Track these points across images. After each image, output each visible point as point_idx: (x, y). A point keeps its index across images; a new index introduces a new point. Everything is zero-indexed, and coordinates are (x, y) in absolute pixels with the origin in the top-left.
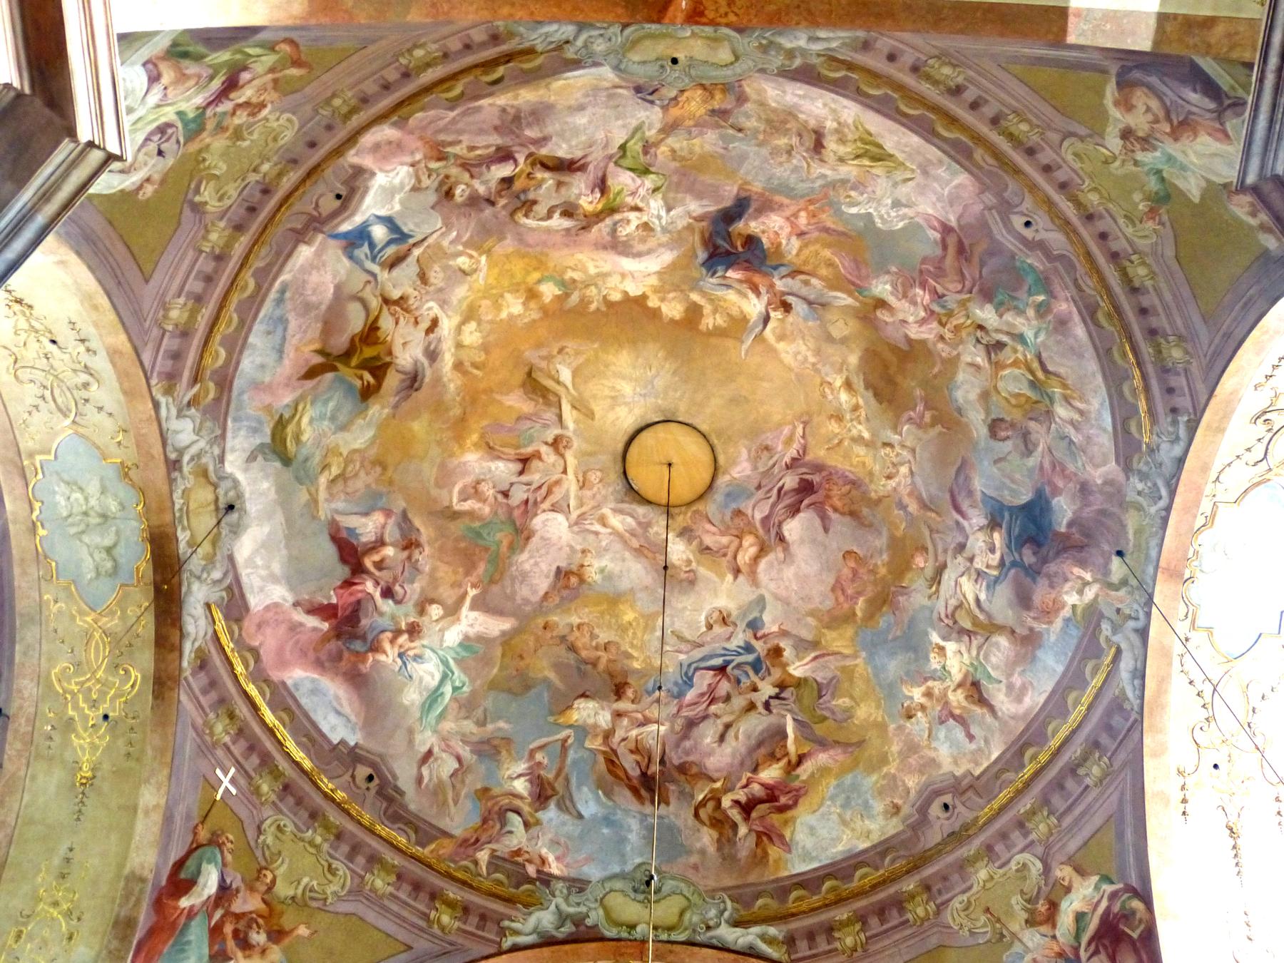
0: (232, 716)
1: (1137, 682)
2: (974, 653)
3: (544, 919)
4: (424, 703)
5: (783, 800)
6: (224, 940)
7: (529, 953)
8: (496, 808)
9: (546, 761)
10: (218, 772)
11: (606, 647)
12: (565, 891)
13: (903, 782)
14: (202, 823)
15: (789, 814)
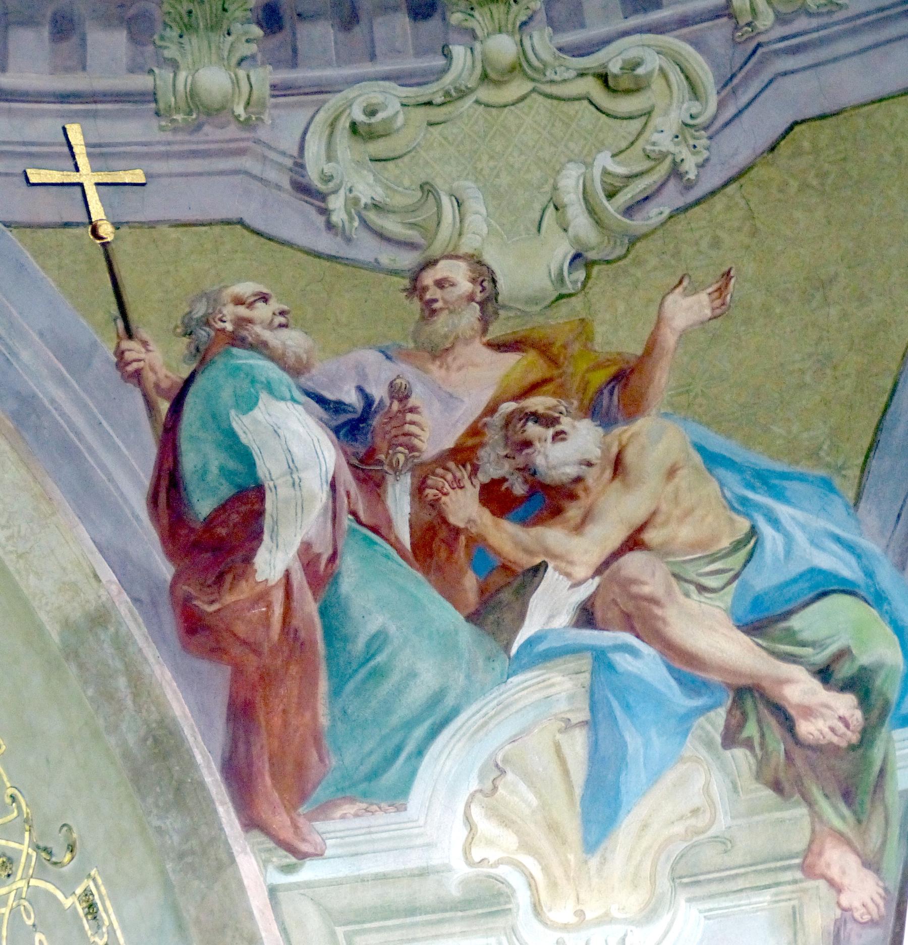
14: (129, 333)
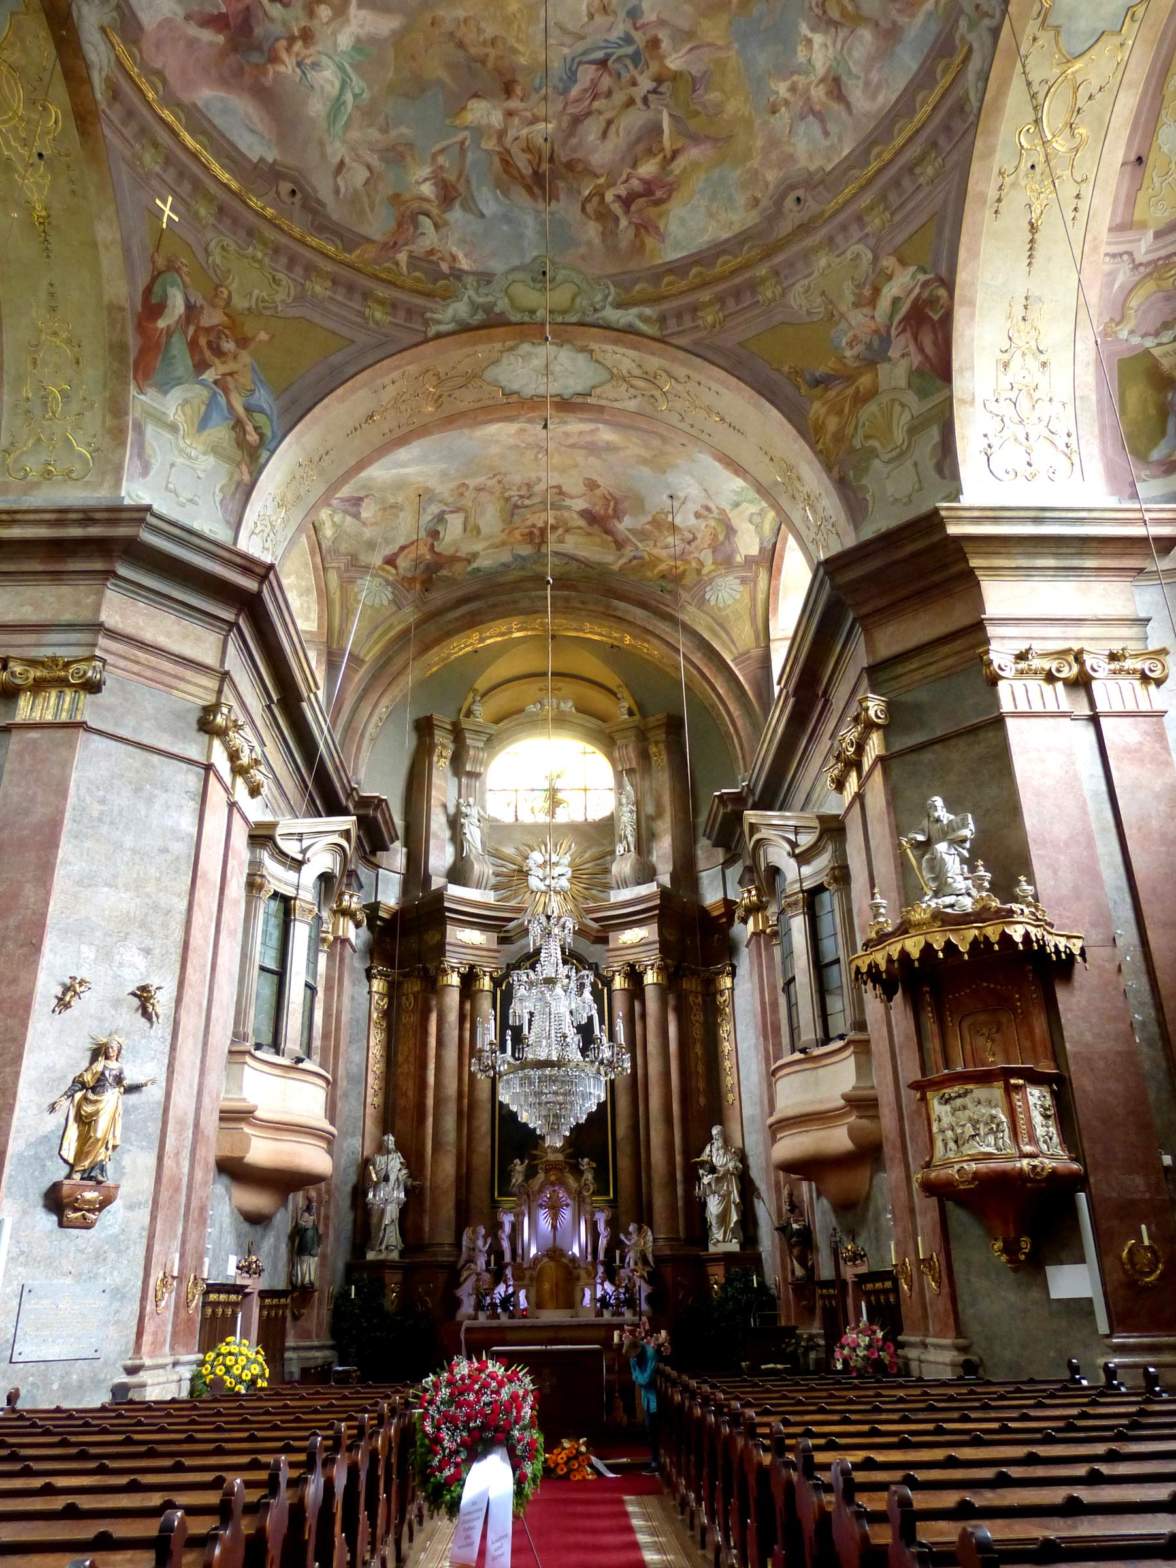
0: (156, 145)
1: (980, 84)
2: (839, 46)
3: (459, 309)
4: (330, 111)
5: (659, 194)
6: (202, 352)
7: (450, 339)
8: (408, 213)
9: (447, 165)
10: (158, 202)
11: (493, 42)
12: (475, 284)
13: (764, 176)
14: (157, 251)
15: (663, 207)
